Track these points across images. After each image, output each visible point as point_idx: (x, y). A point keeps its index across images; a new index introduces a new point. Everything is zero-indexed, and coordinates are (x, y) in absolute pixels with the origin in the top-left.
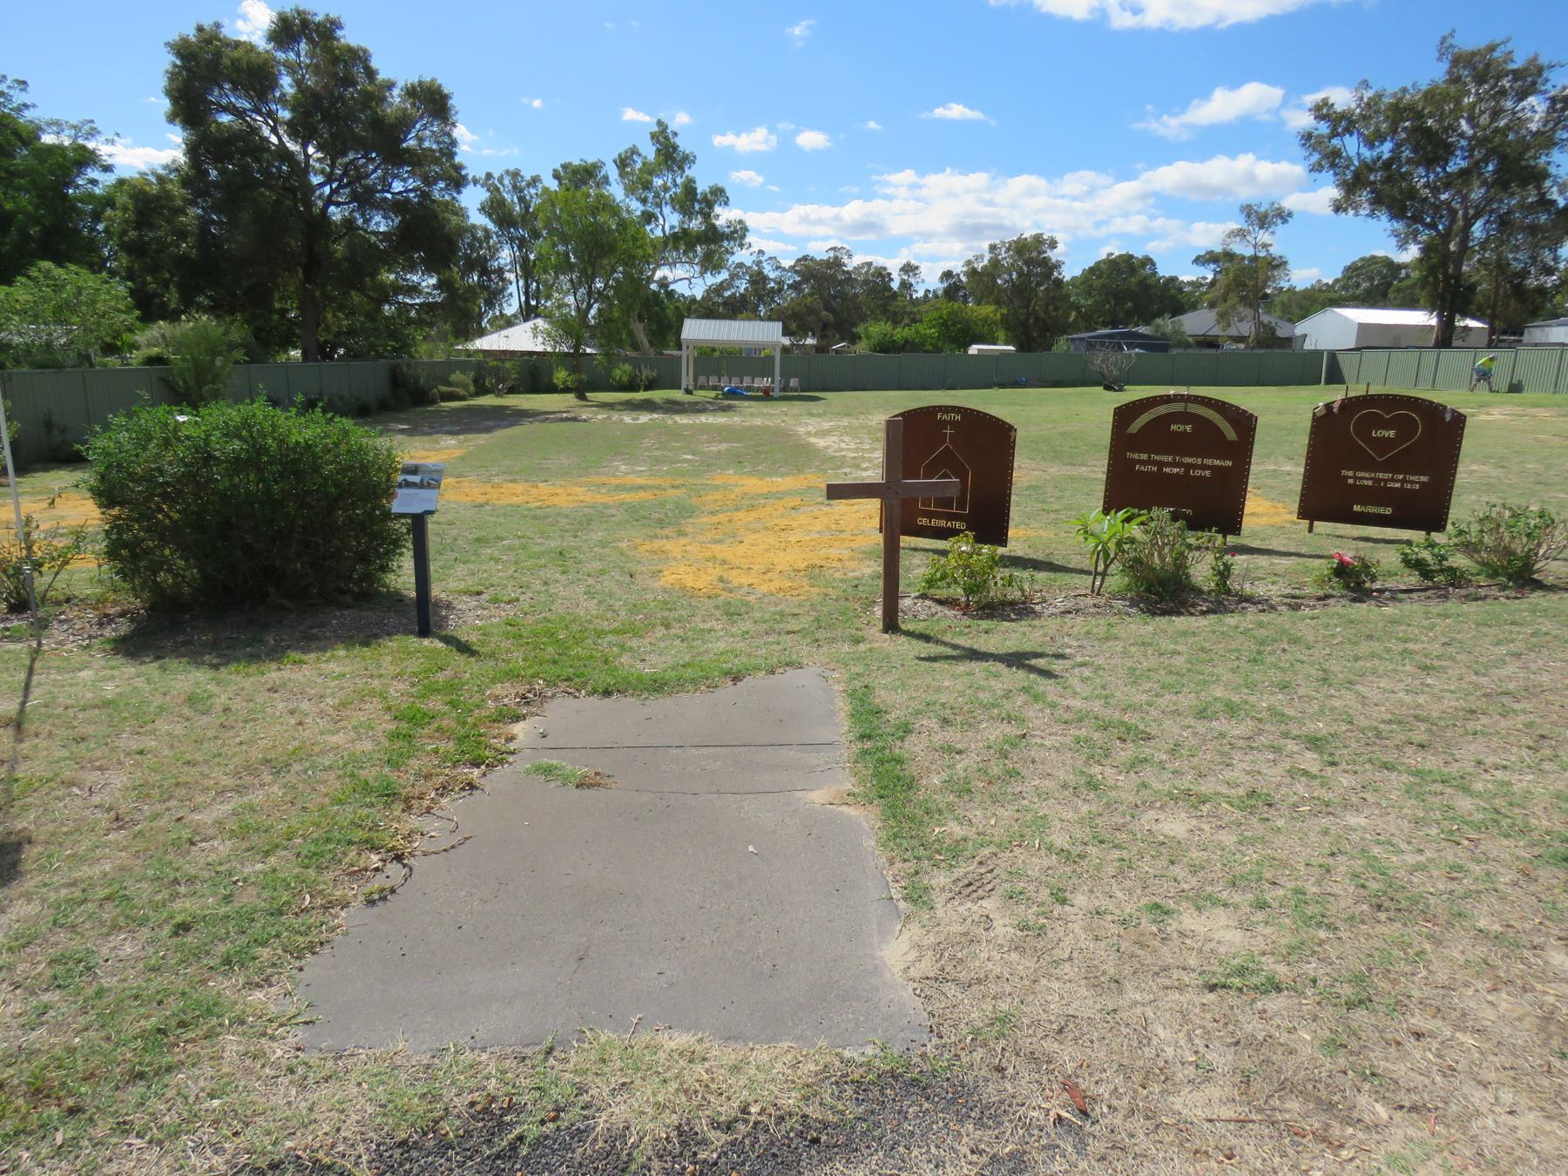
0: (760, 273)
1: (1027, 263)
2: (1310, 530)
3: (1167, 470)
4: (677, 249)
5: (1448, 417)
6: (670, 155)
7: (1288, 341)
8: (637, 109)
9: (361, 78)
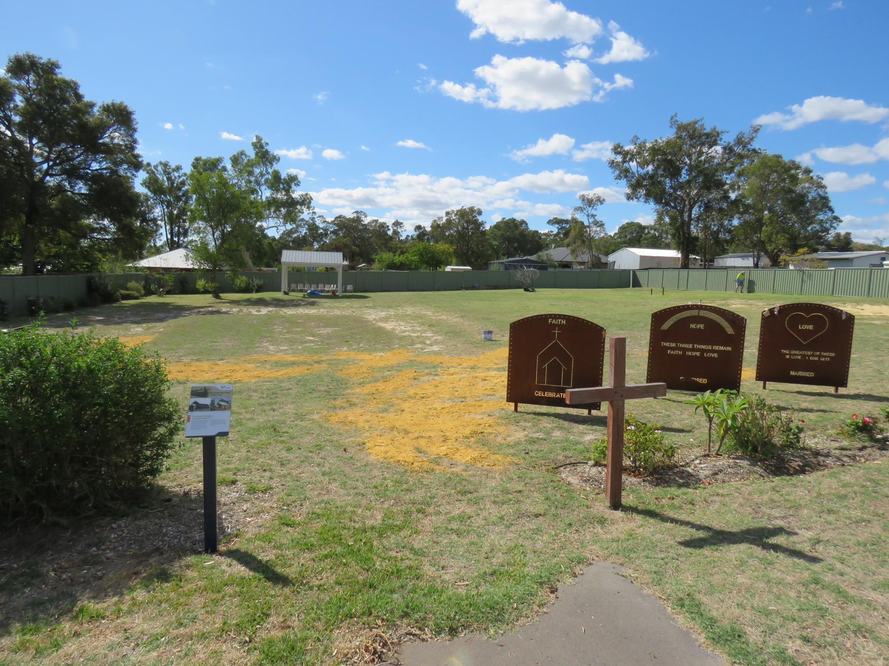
0: (314, 224)
1: (467, 222)
2: (764, 388)
3: (690, 353)
4: (269, 209)
5: (844, 317)
6: (264, 156)
7: (606, 265)
8: (230, 132)
9: (73, 100)
